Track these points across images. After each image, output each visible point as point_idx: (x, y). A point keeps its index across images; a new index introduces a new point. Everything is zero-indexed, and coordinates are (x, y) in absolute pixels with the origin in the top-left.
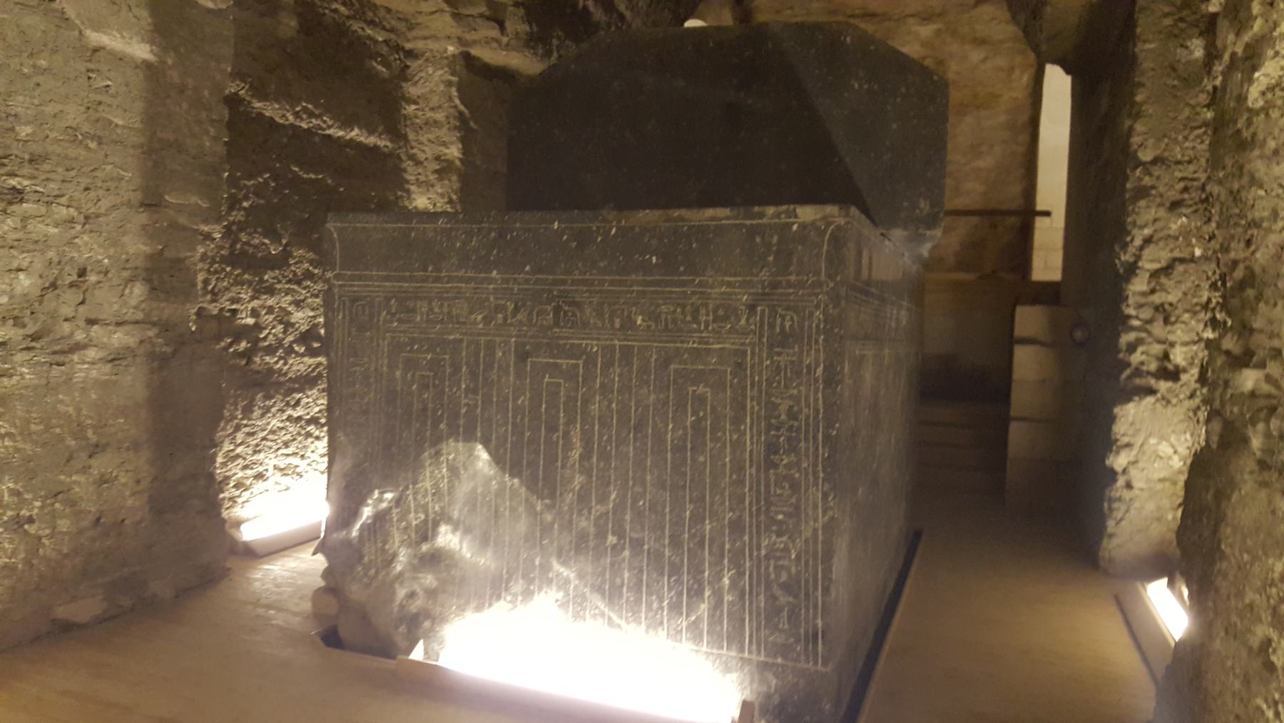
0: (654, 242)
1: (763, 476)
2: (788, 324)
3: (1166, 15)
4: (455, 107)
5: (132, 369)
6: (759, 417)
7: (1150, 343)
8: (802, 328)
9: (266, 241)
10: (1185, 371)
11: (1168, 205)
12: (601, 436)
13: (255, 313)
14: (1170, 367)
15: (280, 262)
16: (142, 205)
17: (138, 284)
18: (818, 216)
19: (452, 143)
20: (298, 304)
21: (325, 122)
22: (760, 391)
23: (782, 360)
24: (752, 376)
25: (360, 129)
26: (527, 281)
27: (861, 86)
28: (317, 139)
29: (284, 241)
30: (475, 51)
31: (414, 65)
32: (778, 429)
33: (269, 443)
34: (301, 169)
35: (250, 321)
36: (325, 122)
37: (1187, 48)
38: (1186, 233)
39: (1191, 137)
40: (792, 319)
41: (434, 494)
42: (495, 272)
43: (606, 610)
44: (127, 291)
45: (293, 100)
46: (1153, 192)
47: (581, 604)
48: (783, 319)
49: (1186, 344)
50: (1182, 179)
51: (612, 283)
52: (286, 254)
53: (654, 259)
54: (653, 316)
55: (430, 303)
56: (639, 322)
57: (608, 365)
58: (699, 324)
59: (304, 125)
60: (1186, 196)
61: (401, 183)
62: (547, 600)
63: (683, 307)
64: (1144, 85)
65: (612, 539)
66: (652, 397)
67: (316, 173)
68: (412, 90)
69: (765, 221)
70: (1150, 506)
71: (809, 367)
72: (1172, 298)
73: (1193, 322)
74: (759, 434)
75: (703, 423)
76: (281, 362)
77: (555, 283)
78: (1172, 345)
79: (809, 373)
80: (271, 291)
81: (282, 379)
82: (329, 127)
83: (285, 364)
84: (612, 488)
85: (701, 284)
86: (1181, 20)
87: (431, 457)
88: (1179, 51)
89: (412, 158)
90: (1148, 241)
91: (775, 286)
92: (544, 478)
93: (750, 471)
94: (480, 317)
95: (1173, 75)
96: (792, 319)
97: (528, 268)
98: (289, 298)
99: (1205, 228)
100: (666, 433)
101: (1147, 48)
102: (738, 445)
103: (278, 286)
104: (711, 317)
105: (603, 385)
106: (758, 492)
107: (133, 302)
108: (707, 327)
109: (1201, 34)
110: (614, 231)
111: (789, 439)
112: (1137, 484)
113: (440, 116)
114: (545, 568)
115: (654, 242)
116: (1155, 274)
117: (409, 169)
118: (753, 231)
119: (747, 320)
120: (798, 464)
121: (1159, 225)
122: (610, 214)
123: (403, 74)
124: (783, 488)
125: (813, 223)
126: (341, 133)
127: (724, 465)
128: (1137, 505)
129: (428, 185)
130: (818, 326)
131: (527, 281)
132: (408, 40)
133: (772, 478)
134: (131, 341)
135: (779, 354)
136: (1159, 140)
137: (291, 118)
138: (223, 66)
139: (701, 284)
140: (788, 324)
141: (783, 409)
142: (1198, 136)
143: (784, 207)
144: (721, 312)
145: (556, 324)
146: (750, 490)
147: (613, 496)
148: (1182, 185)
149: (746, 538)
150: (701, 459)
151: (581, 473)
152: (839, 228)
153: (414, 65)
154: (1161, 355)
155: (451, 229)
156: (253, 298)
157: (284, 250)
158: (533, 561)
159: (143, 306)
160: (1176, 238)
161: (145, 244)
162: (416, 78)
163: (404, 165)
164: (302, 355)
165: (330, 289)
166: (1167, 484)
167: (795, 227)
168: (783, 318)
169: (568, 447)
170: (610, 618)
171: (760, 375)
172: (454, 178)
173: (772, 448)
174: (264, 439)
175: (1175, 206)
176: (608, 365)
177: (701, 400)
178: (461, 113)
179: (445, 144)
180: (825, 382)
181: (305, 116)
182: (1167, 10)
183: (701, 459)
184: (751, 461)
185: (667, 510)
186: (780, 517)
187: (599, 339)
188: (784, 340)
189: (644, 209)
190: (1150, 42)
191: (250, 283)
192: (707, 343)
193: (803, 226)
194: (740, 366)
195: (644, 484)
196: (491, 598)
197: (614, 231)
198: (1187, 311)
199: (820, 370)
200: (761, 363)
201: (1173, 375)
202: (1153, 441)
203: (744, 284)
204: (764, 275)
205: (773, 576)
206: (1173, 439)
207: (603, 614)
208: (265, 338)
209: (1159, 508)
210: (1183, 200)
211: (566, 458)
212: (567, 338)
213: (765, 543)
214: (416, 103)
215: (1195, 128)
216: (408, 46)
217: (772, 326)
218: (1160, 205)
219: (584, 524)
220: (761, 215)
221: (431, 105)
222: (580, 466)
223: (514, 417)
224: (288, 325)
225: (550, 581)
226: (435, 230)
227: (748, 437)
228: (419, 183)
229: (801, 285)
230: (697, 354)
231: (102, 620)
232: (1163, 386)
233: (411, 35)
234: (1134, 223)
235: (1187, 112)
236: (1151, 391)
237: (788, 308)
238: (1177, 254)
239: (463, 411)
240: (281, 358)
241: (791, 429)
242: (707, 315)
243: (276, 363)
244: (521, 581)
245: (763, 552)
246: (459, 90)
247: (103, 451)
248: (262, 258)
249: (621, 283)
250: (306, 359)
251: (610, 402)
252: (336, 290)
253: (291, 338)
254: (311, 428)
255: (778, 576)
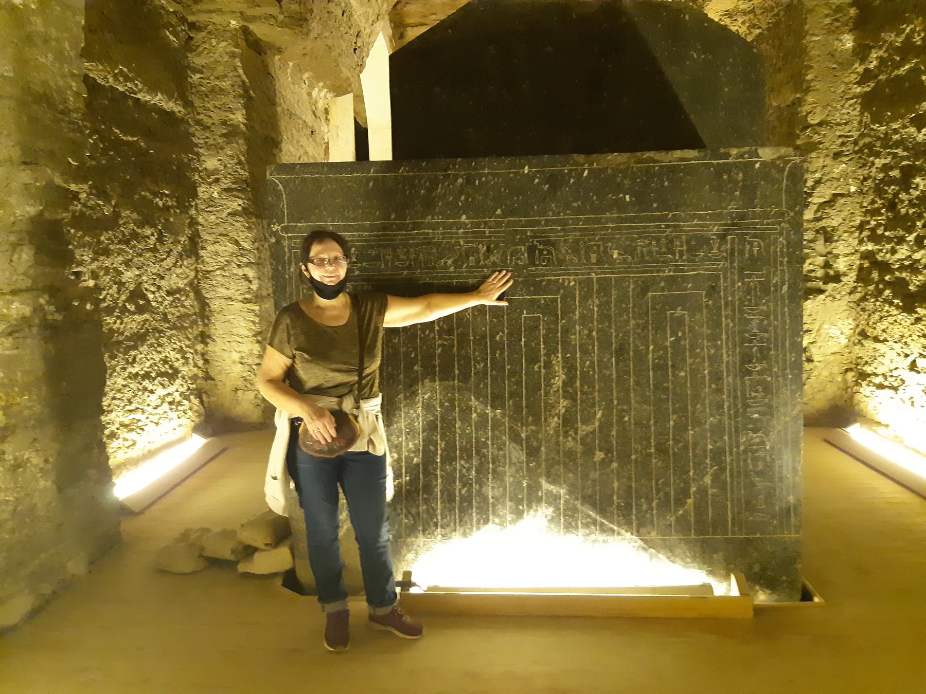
0: (627, 182)
1: (739, 383)
2: (755, 250)
3: (827, 16)
4: (239, 76)
5: (29, 340)
6: (733, 332)
7: (814, 257)
8: (768, 252)
9: (101, 202)
10: (845, 275)
11: (832, 155)
12: (583, 362)
13: (94, 275)
14: (832, 273)
15: (111, 223)
16: (25, 163)
17: (25, 249)
18: (775, 156)
19: (237, 109)
20: (127, 264)
21: (136, 85)
22: (733, 310)
23: (753, 281)
24: (726, 297)
25: (162, 94)
26: (498, 224)
27: (698, 56)
28: (130, 103)
29: (113, 203)
30: (252, 27)
31: (198, 36)
32: (750, 341)
33: (117, 402)
34: (121, 132)
35: (91, 283)
36: (136, 85)
37: (841, 40)
38: (845, 175)
39: (847, 106)
40: (759, 246)
41: (408, 433)
42: (464, 217)
43: (598, 518)
44: (16, 256)
45: (113, 63)
46: (821, 146)
47: (572, 517)
48: (752, 246)
49: (847, 255)
50: (840, 136)
51: (587, 221)
52: (116, 215)
53: (627, 197)
54: (629, 250)
55: (394, 250)
56: (615, 256)
57: (585, 298)
58: (674, 254)
59: (121, 89)
60: (844, 149)
61: (189, 147)
62: (538, 519)
63: (658, 239)
64: (811, 67)
65: (599, 455)
66: (632, 322)
67: (133, 136)
68: (197, 61)
69: (730, 160)
70: (825, 373)
71: (776, 285)
72: (835, 223)
73: (850, 240)
74: (735, 347)
75: (682, 343)
76: (119, 321)
77: (530, 224)
78: (837, 256)
79: (776, 291)
80: (107, 252)
81: (121, 338)
82: (140, 91)
83: (121, 323)
84: (597, 408)
85: (675, 218)
86: (837, 20)
87: (406, 398)
88: (836, 42)
89: (199, 123)
90: (818, 182)
91: (743, 217)
92: (527, 407)
93: (728, 380)
94: (450, 262)
95: (833, 60)
96: (759, 246)
97: (499, 212)
98: (121, 258)
99: (860, 171)
100: (647, 353)
101: (814, 40)
102: (715, 359)
103: (112, 247)
104: (685, 248)
105: (582, 316)
106: (735, 397)
107: (21, 269)
108: (681, 256)
109: (850, 31)
110: (586, 173)
111: (761, 349)
112: (815, 358)
113: (225, 84)
114: (534, 488)
115: (627, 182)
116: (822, 206)
117: (197, 133)
118: (720, 170)
119: (719, 249)
120: (770, 369)
121: (826, 170)
122: (580, 158)
123: (188, 45)
124: (757, 391)
125: (773, 161)
126: (148, 98)
127: (704, 377)
128: (815, 373)
129: (219, 148)
130: (782, 251)
131: (498, 224)
132: (193, 14)
133: (748, 383)
134: (27, 311)
135: (749, 276)
136: (825, 107)
137: (111, 80)
138: (78, 18)
139: (675, 218)
140: (755, 250)
141: (755, 323)
142: (851, 106)
143: (747, 149)
144: (693, 243)
145: (532, 263)
146: (728, 396)
147: (599, 415)
148: (841, 140)
149: (726, 438)
150: (683, 374)
151: (565, 398)
152: (795, 164)
153: (198, 36)
154: (822, 264)
155: (415, 177)
156: (94, 260)
157: (114, 211)
158: (520, 483)
159: (31, 272)
160: (838, 180)
161: (32, 205)
162: (200, 49)
163: (192, 130)
164: (133, 313)
165: (278, 242)
166: (837, 356)
167: (757, 165)
168: (751, 243)
169: (550, 375)
170: (602, 524)
171: (733, 295)
172: (241, 142)
173: (747, 358)
174: (114, 398)
175: (837, 155)
176: (585, 298)
177: (680, 322)
178: (243, 82)
179: (230, 110)
180: (789, 298)
181: (121, 79)
182: (826, 12)
183: (683, 374)
184: (728, 371)
185: (652, 422)
186: (756, 416)
187: (576, 274)
188: (755, 263)
189: (613, 152)
190: (817, 35)
191: (89, 245)
192: (682, 271)
193: (764, 164)
194: (713, 290)
195: (628, 402)
196: (478, 523)
197: (586, 173)
198: (845, 232)
199: (785, 288)
200: (733, 284)
201: (837, 278)
202: (825, 326)
203: (713, 217)
204: (732, 208)
205: (751, 466)
206: (840, 323)
207: (595, 522)
208: (104, 300)
209: (831, 374)
210: (842, 151)
211: (549, 385)
212: (544, 275)
213: (743, 440)
214: (202, 73)
215: (848, 99)
216: (191, 18)
217: (741, 253)
218: (827, 156)
219: (570, 444)
220: (727, 156)
221: (216, 74)
222: (565, 391)
223: (493, 353)
224: (121, 284)
225: (539, 500)
226: (396, 178)
227: (724, 351)
228: (208, 147)
229: (766, 215)
230: (672, 281)
231: (35, 613)
232: (830, 286)
233: (195, 8)
234: (807, 170)
235: (842, 88)
236: (821, 291)
237: (755, 236)
238: (838, 191)
239: (439, 351)
240: (118, 317)
241: (761, 340)
242: (682, 246)
243: (115, 323)
244: (509, 503)
245: (742, 448)
246: (241, 61)
247: (13, 433)
248: (97, 219)
249: (597, 221)
250: (136, 317)
251: (591, 331)
252: (286, 243)
253: (123, 298)
254: (146, 383)
255: (755, 466)
